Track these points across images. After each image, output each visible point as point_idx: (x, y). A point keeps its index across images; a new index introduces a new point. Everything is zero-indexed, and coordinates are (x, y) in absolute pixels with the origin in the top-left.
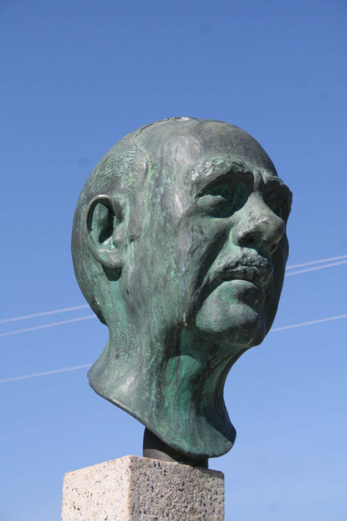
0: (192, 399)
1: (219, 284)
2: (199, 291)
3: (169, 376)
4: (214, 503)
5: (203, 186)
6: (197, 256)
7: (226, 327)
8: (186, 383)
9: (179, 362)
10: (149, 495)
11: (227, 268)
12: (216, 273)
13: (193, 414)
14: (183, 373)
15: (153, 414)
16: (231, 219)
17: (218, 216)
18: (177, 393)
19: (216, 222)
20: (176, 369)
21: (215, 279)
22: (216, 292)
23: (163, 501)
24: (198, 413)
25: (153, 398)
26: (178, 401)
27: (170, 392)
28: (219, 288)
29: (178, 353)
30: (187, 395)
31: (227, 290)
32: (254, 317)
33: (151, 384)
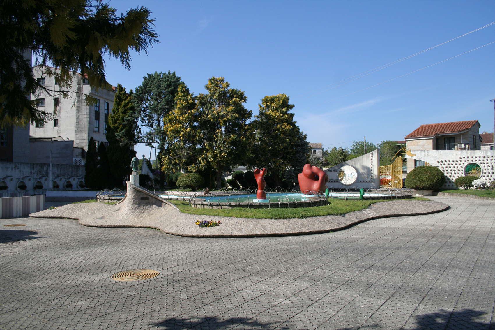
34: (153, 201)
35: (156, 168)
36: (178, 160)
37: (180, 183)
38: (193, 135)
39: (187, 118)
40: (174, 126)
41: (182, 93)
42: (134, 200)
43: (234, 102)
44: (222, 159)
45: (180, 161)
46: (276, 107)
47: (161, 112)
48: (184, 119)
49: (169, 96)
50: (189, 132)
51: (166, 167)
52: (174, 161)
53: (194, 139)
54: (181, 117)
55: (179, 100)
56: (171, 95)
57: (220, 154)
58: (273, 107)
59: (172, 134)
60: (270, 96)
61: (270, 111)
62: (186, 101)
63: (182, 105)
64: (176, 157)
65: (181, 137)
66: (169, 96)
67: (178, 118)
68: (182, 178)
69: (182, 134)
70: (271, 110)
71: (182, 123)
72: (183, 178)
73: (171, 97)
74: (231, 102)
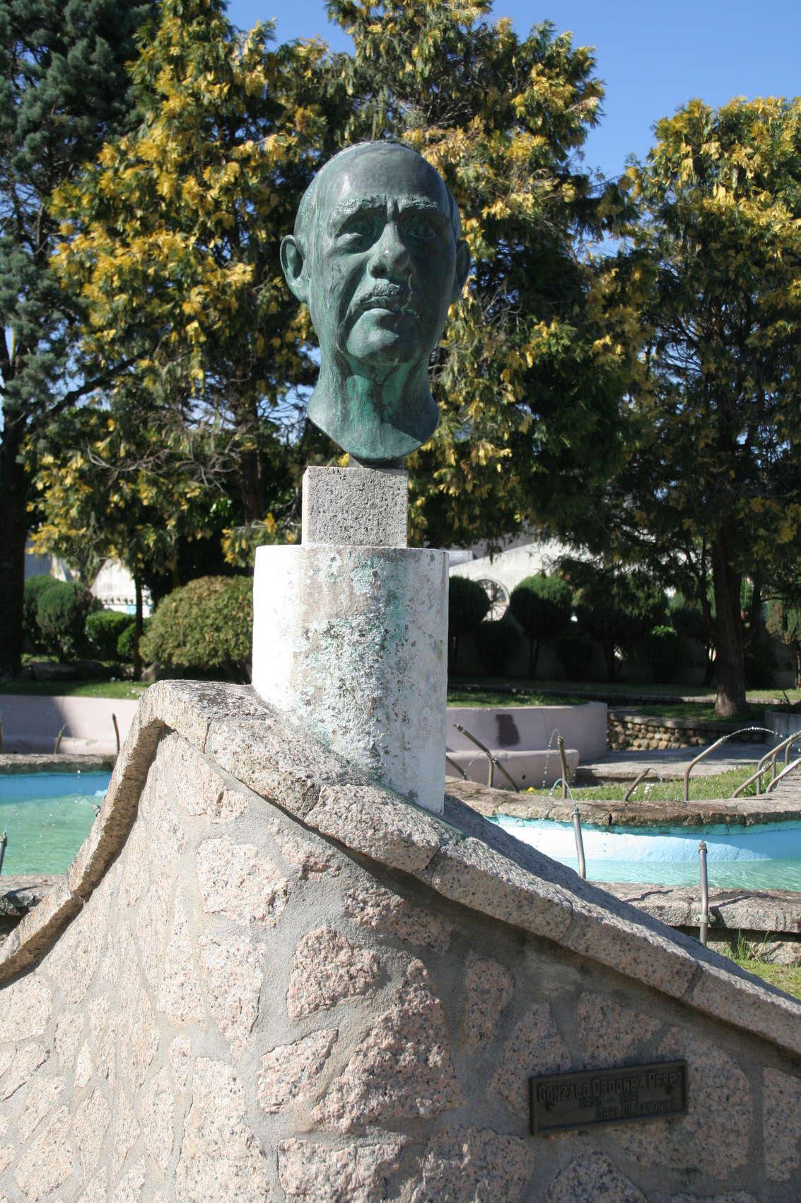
0: (375, 410)
1: (362, 314)
2: (343, 323)
3: (350, 393)
4: (396, 498)
5: (339, 227)
6: (336, 293)
7: (366, 353)
8: (365, 398)
9: (354, 381)
10: (328, 497)
11: (363, 301)
12: (356, 305)
13: (377, 423)
14: (360, 389)
15: (477, 393)
16: (368, 252)
17: (358, 251)
18: (359, 407)
19: (355, 258)
20: (354, 387)
21: (356, 311)
22: (359, 321)
23: (343, 501)
24: (382, 421)
25: (338, 413)
26: (361, 413)
27: (354, 406)
28: (362, 317)
29: (351, 374)
30: (369, 407)
31: (367, 319)
32: (392, 340)
33: (337, 401)
34: (757, 1149)
35: (401, 483)
36: (153, 482)
37: (171, 643)
38: (269, 319)
39: (226, 190)
40: (137, 246)
41: (187, 19)
42: (388, 1147)
43: (537, 108)
44: (469, 487)
45: (169, 493)
46: (758, 177)
47: (34, 149)
48: (214, 193)
49: (92, 46)
50: (245, 294)
51: (64, 530)
52: (731, 360)
53: (276, 342)
54: (191, 183)
55: (168, 69)
56: (102, 44)
57: (463, 451)
58: (742, 172)
59: (121, 299)
60: (717, 103)
61: (722, 197)
62: (222, 70)
63: (196, 96)
64: (144, 468)
65: (190, 319)
66: (92, 46)
67: (165, 188)
68: (185, 607)
69: (195, 299)
70: (728, 188)
71: (188, 230)
72: (195, 610)
73: (105, 55)
74: (518, 100)
